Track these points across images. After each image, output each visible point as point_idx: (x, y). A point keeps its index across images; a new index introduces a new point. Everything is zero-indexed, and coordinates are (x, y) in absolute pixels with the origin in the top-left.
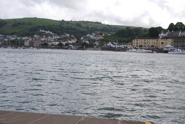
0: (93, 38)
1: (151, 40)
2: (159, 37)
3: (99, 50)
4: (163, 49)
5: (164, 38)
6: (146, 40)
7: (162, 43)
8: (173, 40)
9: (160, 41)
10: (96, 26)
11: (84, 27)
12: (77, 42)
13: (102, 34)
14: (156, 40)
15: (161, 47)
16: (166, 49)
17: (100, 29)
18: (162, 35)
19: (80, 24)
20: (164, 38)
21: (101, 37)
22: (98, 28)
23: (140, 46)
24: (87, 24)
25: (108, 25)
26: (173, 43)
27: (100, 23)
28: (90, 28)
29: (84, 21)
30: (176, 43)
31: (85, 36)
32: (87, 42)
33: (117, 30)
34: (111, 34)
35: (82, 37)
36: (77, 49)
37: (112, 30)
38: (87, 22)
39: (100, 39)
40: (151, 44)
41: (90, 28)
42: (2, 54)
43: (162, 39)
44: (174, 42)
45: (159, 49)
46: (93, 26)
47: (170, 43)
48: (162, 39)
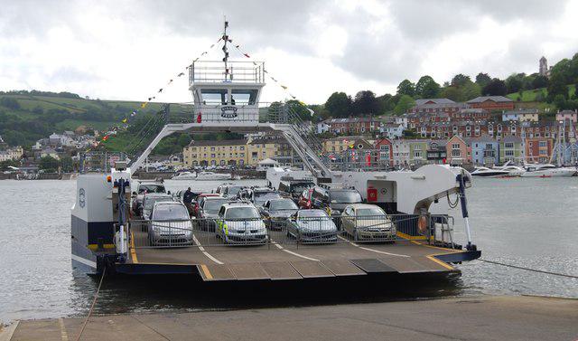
0: (68, 144)
1: (227, 148)
6: (216, 148)
7: (255, 154)
9: (249, 148)
11: (28, 111)
12: (24, 156)
14: (238, 147)
15: (251, 162)
17: (76, 114)
18: (250, 137)
20: (255, 142)
27: (75, 97)
28: (45, 111)
29: (25, 93)
30: (286, 153)
31: (46, 140)
32: (54, 156)
35: (38, 143)
36: (39, 178)
38: (35, 93)
41: (45, 111)
43: (252, 144)
44: (282, 149)
45: (246, 168)
47: (271, 153)
48: (252, 144)
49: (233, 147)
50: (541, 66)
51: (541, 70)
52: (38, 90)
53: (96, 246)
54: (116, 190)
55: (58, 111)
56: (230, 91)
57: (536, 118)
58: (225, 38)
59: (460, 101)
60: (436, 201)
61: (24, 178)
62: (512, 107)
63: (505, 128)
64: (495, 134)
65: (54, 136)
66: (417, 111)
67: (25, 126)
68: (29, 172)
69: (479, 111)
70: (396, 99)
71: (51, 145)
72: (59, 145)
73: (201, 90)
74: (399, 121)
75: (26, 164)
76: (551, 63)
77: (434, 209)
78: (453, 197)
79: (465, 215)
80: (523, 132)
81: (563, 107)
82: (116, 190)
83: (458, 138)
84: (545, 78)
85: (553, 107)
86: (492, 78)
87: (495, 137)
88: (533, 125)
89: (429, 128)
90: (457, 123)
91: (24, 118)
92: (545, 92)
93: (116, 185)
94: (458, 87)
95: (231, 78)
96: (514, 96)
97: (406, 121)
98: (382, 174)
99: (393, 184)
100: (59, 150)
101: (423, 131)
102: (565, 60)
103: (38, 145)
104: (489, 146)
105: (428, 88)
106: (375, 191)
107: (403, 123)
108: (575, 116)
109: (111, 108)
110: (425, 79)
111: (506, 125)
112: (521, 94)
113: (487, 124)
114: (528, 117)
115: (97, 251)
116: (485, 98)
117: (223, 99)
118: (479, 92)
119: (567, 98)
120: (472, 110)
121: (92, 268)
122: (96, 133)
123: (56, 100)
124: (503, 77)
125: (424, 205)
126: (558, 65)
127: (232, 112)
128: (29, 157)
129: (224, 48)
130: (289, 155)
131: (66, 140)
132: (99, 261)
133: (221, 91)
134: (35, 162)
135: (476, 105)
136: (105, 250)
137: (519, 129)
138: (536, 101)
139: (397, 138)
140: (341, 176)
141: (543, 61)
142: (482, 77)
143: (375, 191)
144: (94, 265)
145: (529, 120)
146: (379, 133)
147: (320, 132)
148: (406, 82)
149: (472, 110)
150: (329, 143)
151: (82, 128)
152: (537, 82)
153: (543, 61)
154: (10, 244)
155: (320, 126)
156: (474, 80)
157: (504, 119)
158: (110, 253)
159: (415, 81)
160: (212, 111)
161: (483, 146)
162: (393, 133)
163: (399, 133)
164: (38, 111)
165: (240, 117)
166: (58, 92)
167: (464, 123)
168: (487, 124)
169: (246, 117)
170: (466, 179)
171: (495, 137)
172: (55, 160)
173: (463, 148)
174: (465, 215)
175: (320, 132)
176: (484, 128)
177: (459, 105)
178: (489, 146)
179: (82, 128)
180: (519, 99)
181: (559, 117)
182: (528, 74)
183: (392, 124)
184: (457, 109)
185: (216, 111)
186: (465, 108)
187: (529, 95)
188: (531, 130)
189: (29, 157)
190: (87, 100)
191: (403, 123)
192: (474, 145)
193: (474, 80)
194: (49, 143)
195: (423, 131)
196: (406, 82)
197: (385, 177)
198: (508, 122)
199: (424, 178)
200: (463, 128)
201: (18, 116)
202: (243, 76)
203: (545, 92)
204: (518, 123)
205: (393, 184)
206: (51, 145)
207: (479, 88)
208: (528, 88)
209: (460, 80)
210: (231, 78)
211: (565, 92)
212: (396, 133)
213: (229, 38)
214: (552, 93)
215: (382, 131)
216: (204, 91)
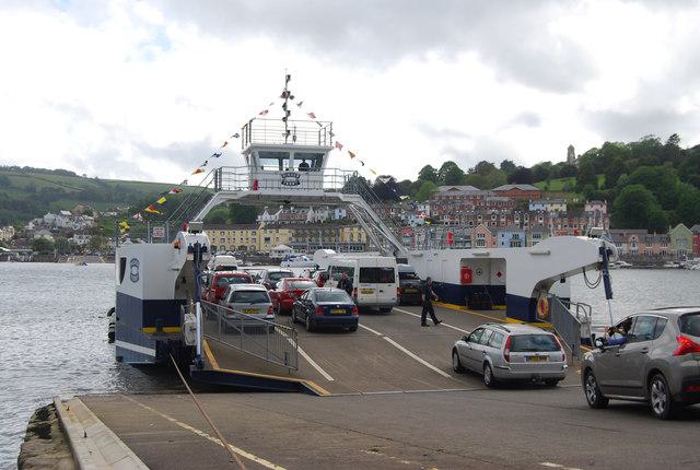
0: (64, 225)
1: (238, 232)
2: (258, 224)
3: (100, 262)
4: (268, 254)
5: (270, 226)
6: (226, 232)
7: (267, 239)
8: (293, 231)
9: (261, 234)
10: (60, 183)
11: (19, 189)
12: (15, 237)
13: (90, 214)
14: (250, 232)
15: (263, 248)
16: (276, 256)
17: (73, 193)
18: (265, 217)
19: (6, 178)
20: (270, 226)
21: (89, 223)
22: (68, 190)
23: (683, 330)
24: (28, 176)
25: (97, 180)
26: (294, 240)
27: (72, 174)
28: (39, 189)
29: (17, 169)
30: (300, 239)
31: (40, 220)
32: (49, 237)
33: (127, 195)
34: (116, 210)
35: (31, 223)
36: (33, 261)
37: (114, 198)
38: (27, 169)
39: (87, 227)
40: (238, 243)
41: (39, 189)
42: (5, 331)
43: (265, 228)
44: (296, 236)
45: (258, 254)
46: (48, 185)
47: (284, 239)
48: (265, 228)
49: (244, 232)
50: (569, 154)
51: (569, 158)
52: (31, 166)
53: (153, 330)
54: (191, 257)
55: (52, 189)
56: (292, 156)
57: (564, 208)
58: (286, 95)
59: (486, 188)
60: (563, 281)
61: (17, 260)
62: (540, 196)
63: (532, 218)
64: (522, 224)
65: (49, 217)
66: (440, 198)
67: (15, 205)
68: (20, 253)
69: (506, 199)
70: (417, 185)
71: (44, 225)
72: (54, 225)
73: (257, 154)
74: (421, 208)
75: (18, 245)
76: (580, 151)
77: (557, 289)
78: (594, 275)
79: (609, 295)
80: (551, 222)
81: (592, 198)
82: (191, 257)
83: (483, 228)
84: (573, 167)
85: (582, 197)
86: (517, 165)
87: (522, 227)
88: (561, 215)
89: (452, 216)
90: (480, 211)
91: (15, 196)
92: (574, 181)
93: (191, 250)
94: (482, 174)
95: (294, 139)
96: (541, 185)
97: (428, 207)
98: (481, 250)
99: (503, 261)
100: (54, 232)
101: (446, 220)
102: (549, 163)
103: (31, 226)
104: (516, 237)
105: (452, 174)
106: (470, 272)
107: (425, 209)
108: (605, 207)
109: (110, 187)
110: (448, 165)
111: (533, 214)
112: (548, 183)
113: (513, 213)
114: (556, 207)
115: (154, 334)
116: (511, 187)
117: (281, 164)
118: (504, 180)
119: (597, 189)
120: (498, 199)
121: (149, 357)
122: (95, 213)
123: (53, 178)
124: (529, 164)
125: (543, 286)
126: (586, 154)
127: (294, 179)
128: (21, 239)
129: (285, 106)
130: (304, 241)
131: (63, 222)
132: (159, 346)
133: (280, 154)
134: (26, 244)
135: (502, 193)
136: (165, 334)
137: (547, 219)
138: (564, 190)
139: (419, 225)
140: (422, 255)
141: (571, 149)
142: (507, 165)
143: (470, 272)
144: (152, 352)
145: (556, 210)
146: (400, 220)
147: (337, 218)
148: (428, 167)
149: (498, 199)
150: (347, 230)
151: (81, 207)
152: (565, 170)
153: (571, 149)
154: (51, 329)
155: (337, 211)
156: (498, 166)
157: (531, 208)
158: (174, 338)
159: (437, 166)
160: (270, 177)
161: (509, 236)
162: (414, 220)
163: (421, 221)
164: (31, 189)
165: (305, 185)
166: (53, 169)
167: (490, 212)
168: (513, 213)
169: (311, 185)
170: (610, 252)
171: (522, 227)
172: (49, 243)
173: (488, 238)
174: (609, 295)
175: (337, 218)
176: (510, 218)
177: (484, 193)
178: (516, 237)
179: (81, 207)
180: (546, 188)
181: (588, 208)
182: (554, 163)
183: (414, 210)
184: (482, 196)
185: (274, 177)
186: (491, 196)
187: (557, 184)
188: (559, 221)
189: (21, 239)
190: (85, 178)
191: (425, 209)
192: (500, 234)
193: (498, 166)
194: (43, 223)
195: (447, 219)
196: (428, 167)
197: (488, 254)
198: (533, 212)
199: (549, 253)
200: (488, 217)
201: (9, 195)
202: (308, 139)
203: (574, 181)
204: (546, 213)
205: (503, 261)
206: (44, 225)
207: (505, 176)
208: (556, 177)
209: (484, 168)
210: (294, 139)
211: (594, 181)
212: (417, 221)
213: (291, 94)
214: (581, 182)
215: (403, 218)
216: (263, 155)
